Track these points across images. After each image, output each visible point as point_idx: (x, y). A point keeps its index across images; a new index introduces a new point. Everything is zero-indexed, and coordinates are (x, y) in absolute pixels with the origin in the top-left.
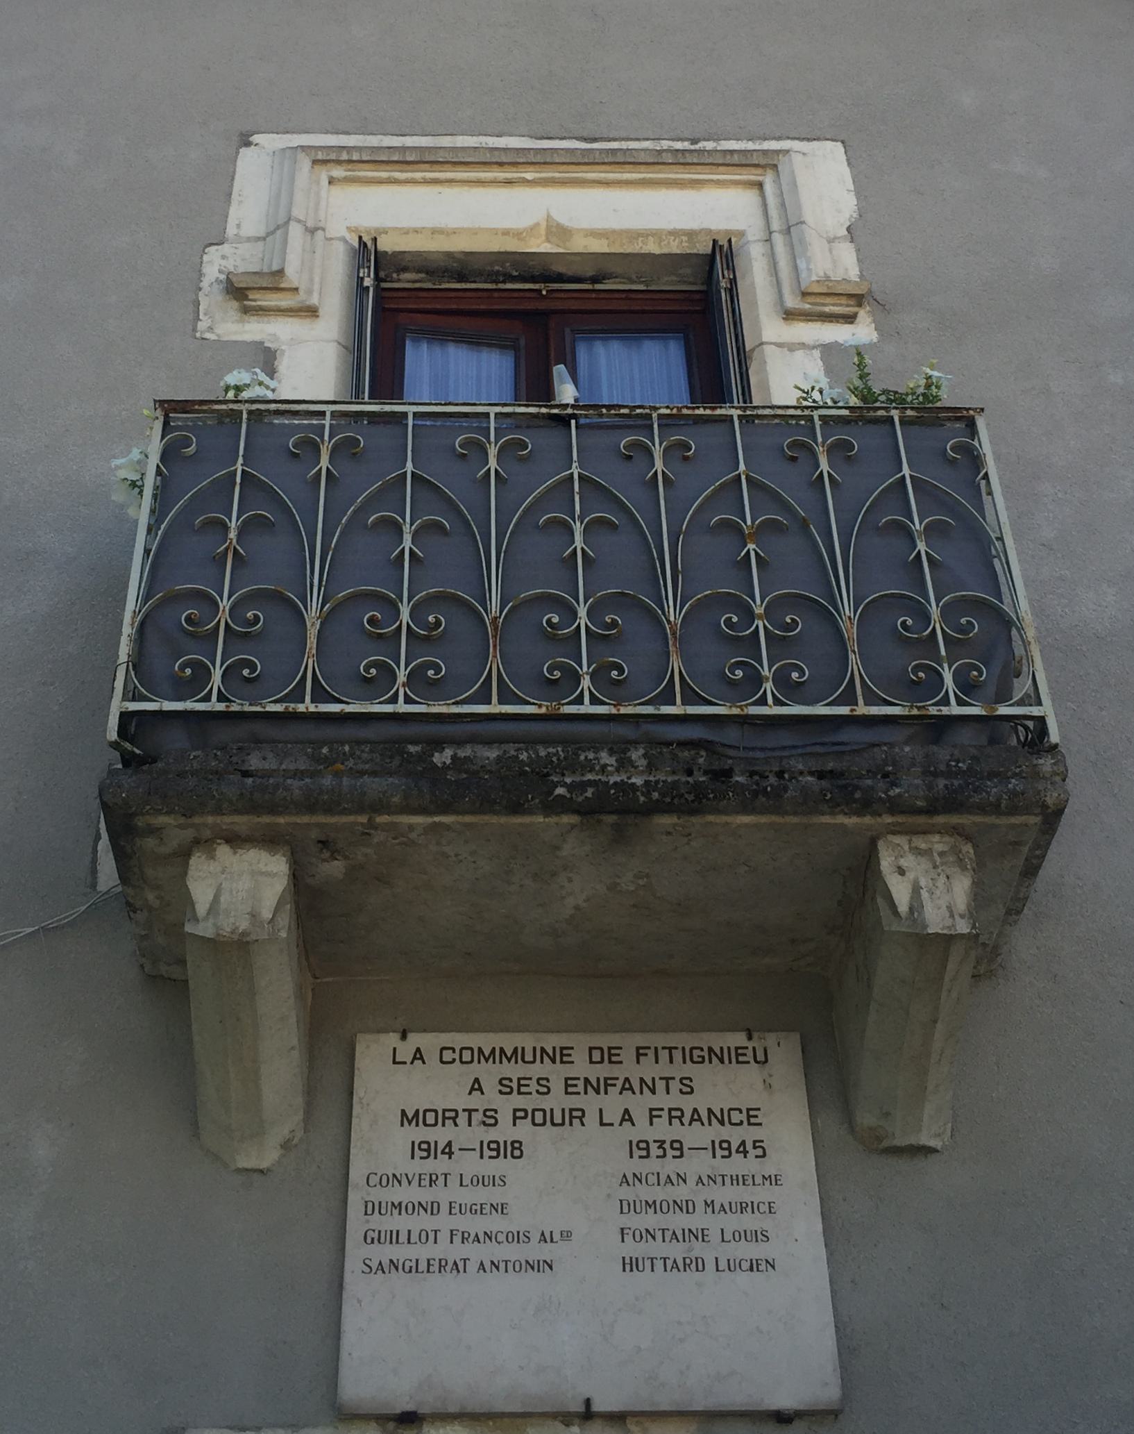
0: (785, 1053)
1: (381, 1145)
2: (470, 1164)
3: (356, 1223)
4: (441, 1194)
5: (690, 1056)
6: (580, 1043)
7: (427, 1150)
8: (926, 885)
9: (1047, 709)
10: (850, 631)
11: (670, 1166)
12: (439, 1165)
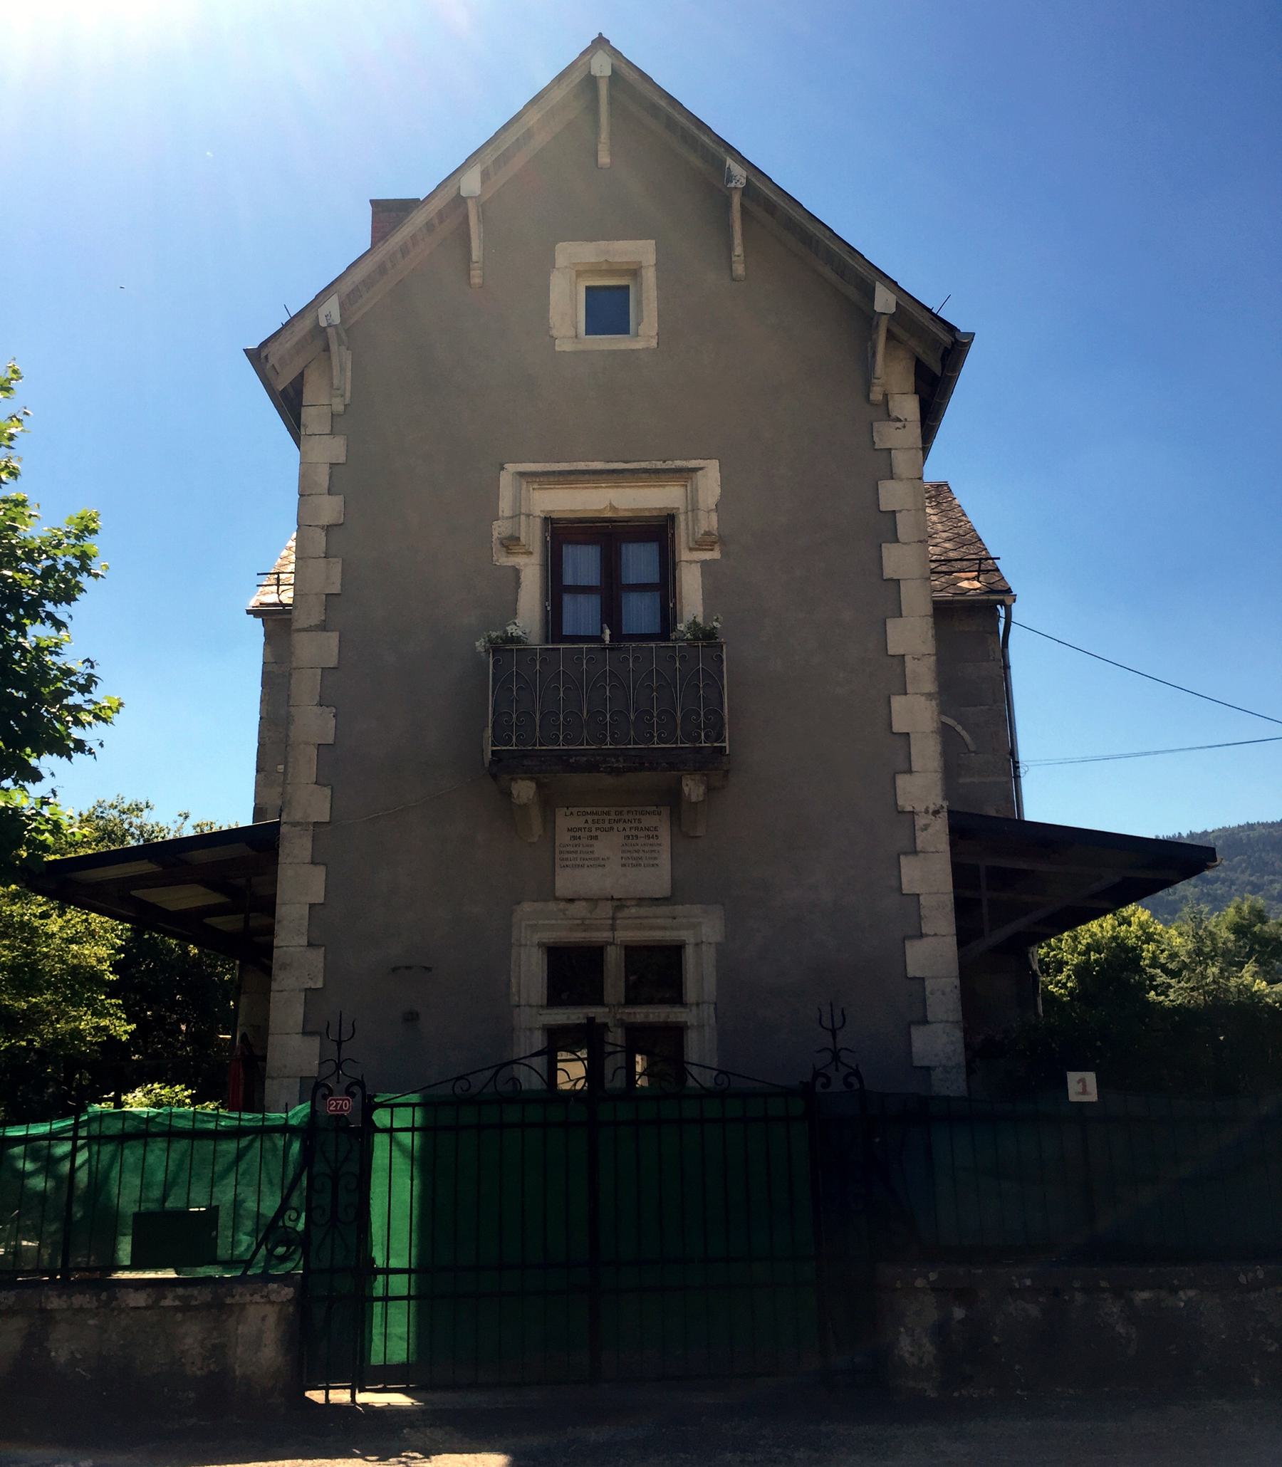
0: (665, 811)
1: (563, 837)
2: (584, 841)
3: (557, 856)
4: (578, 849)
5: (641, 813)
6: (613, 810)
7: (574, 838)
8: (693, 789)
9: (726, 744)
10: (679, 722)
11: (634, 842)
12: (577, 842)
